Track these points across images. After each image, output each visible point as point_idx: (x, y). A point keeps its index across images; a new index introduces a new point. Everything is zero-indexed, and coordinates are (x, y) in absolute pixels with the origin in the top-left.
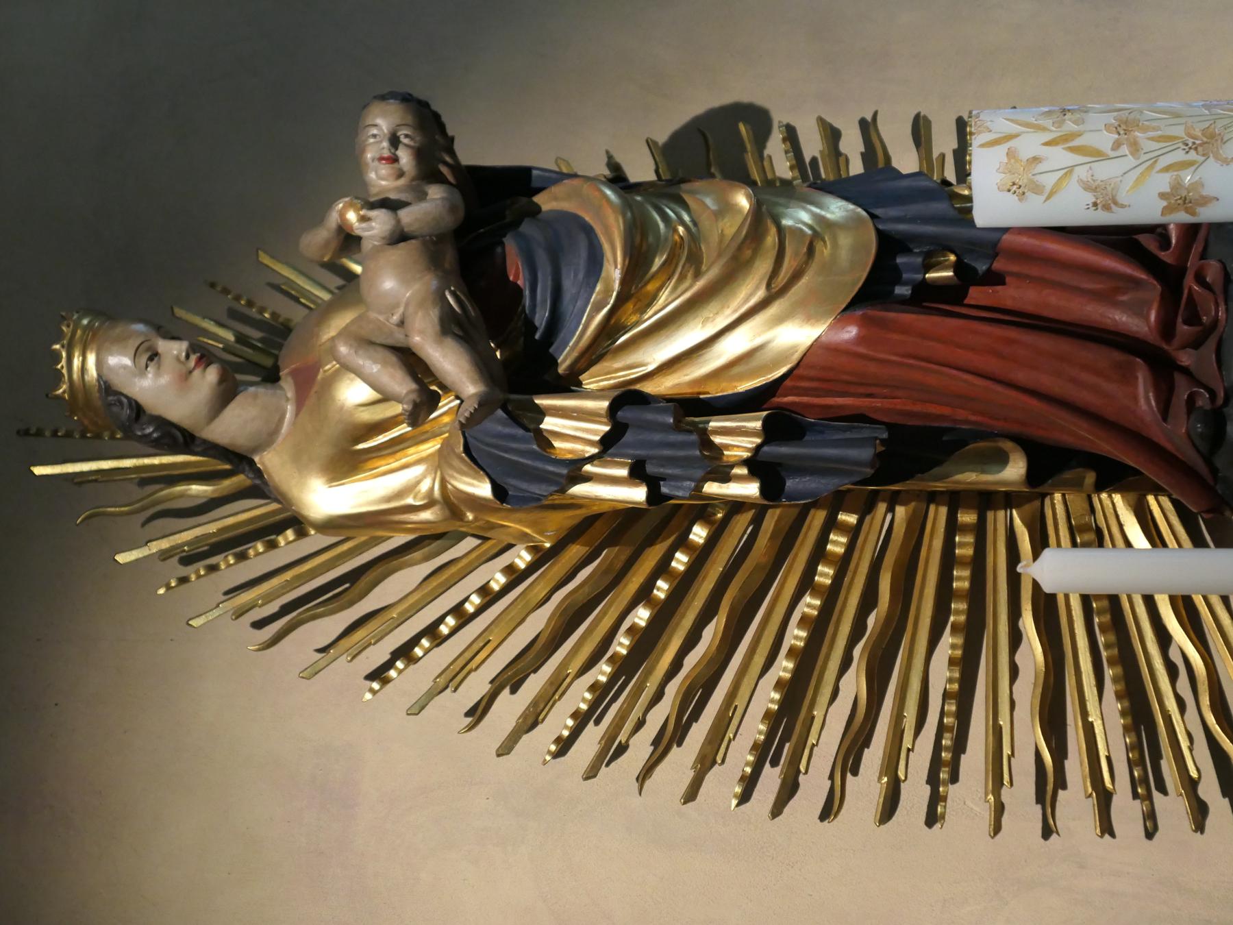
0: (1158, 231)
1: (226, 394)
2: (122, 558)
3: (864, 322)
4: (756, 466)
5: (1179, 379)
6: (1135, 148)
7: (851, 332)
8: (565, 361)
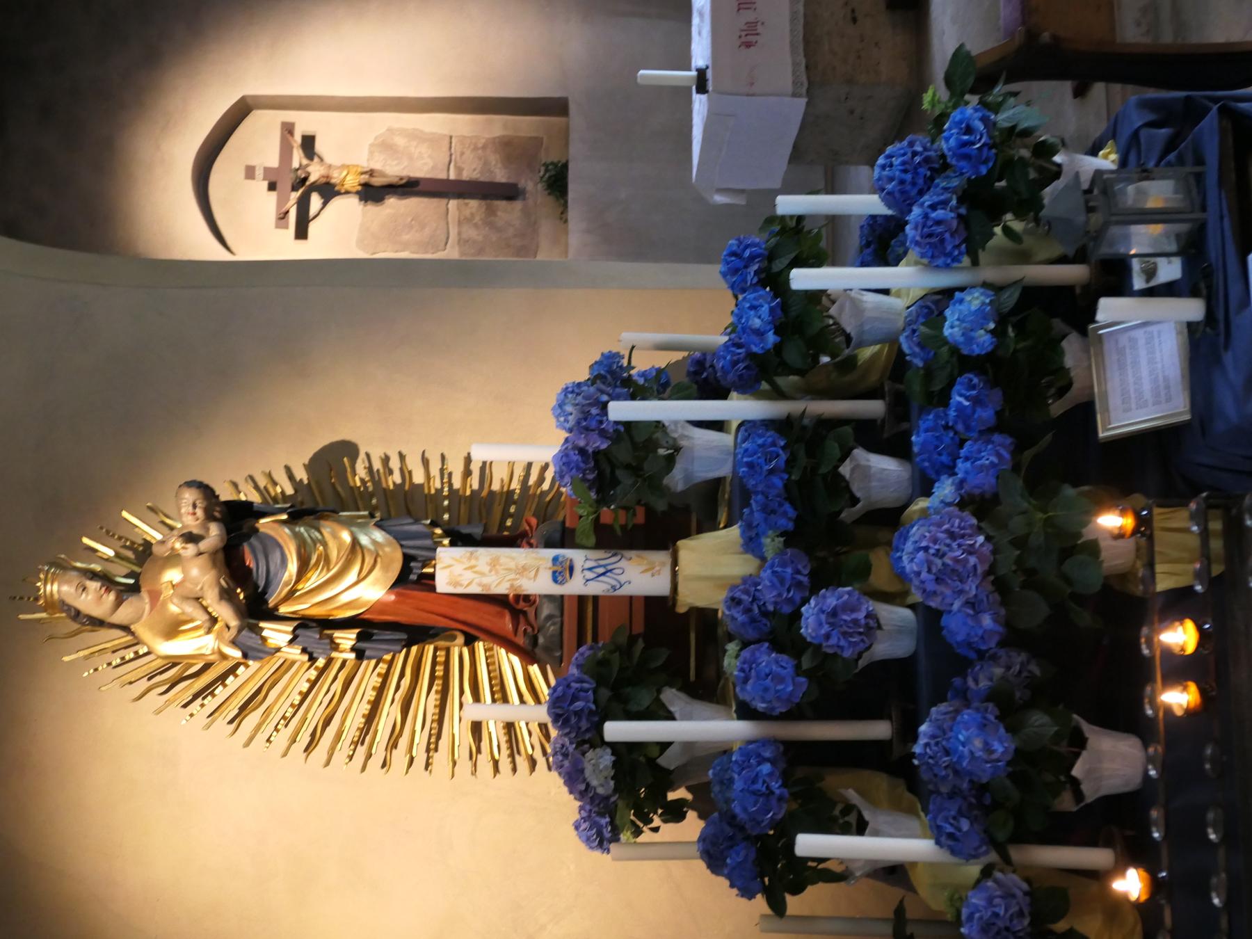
0: (506, 596)
1: (119, 603)
2: (66, 659)
3: (398, 595)
4: (353, 649)
5: (522, 619)
6: (497, 572)
7: (393, 597)
8: (272, 602)
